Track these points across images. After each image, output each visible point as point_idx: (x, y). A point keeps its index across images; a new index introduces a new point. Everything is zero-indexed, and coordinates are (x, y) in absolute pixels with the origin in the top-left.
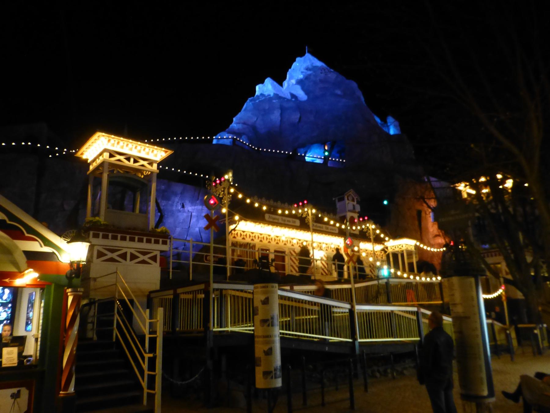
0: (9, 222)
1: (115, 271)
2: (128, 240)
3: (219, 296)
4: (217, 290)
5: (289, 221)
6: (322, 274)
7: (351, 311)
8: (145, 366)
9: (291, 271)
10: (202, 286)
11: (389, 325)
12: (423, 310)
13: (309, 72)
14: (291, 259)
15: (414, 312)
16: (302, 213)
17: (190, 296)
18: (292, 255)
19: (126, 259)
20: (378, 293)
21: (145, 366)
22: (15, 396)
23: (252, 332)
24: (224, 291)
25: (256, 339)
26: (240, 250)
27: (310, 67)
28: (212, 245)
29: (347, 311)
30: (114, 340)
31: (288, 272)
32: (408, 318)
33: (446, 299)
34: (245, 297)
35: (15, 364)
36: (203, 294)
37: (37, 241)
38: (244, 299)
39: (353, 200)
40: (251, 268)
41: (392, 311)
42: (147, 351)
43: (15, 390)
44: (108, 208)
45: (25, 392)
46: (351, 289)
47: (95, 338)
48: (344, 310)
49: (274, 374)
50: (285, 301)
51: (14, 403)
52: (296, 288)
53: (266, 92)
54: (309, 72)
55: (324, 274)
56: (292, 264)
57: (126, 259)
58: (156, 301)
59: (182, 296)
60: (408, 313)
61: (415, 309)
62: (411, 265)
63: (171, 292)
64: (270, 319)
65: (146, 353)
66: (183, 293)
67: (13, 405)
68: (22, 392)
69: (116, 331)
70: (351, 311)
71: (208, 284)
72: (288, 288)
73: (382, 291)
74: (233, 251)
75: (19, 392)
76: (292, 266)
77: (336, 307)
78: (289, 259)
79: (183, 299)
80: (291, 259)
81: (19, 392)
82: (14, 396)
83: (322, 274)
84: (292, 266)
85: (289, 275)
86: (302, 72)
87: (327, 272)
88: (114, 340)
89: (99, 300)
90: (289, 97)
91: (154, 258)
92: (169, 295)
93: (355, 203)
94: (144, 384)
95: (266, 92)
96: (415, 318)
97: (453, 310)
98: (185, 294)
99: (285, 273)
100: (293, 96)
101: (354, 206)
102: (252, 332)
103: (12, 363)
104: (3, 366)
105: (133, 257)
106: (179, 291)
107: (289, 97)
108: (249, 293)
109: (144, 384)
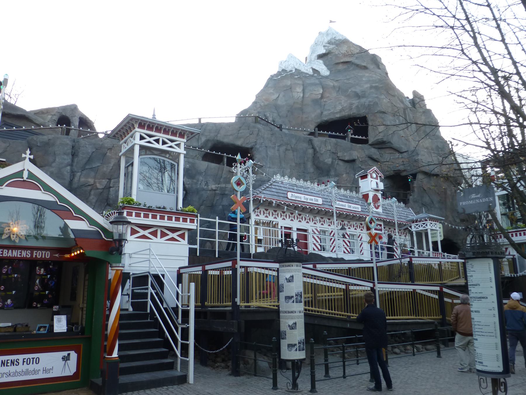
0: (59, 203)
1: (149, 248)
2: (190, 247)
3: (342, 297)
4: (243, 267)
5: (312, 200)
6: (344, 252)
7: (373, 289)
8: (179, 337)
9: (314, 250)
10: (229, 264)
11: (410, 302)
12: (445, 290)
13: (331, 47)
14: (313, 237)
15: (436, 291)
17: (217, 273)
18: (315, 233)
19: (156, 237)
20: (400, 271)
21: (179, 337)
22: (66, 359)
23: (277, 308)
24: (248, 268)
25: (281, 314)
26: (263, 229)
27: (333, 41)
28: (238, 224)
29: (369, 289)
30: (149, 311)
31: (310, 250)
32: (427, 296)
35: (65, 330)
36: (441, 315)
37: (84, 220)
39: (377, 178)
40: (274, 246)
42: (180, 322)
43: (65, 353)
45: (74, 355)
47: (131, 309)
48: (366, 288)
49: (298, 346)
50: (434, 295)
51: (65, 364)
53: (287, 68)
54: (331, 47)
56: (315, 242)
57: (156, 237)
58: (185, 277)
59: (210, 273)
60: (433, 293)
61: (438, 288)
62: (435, 243)
63: (200, 268)
64: (295, 296)
65: (179, 324)
66: (211, 270)
67: (479, 81)
68: (71, 355)
69: (150, 302)
71: (235, 262)
72: (311, 266)
73: (405, 270)
74: (256, 229)
75: (69, 354)
76: (315, 244)
78: (312, 236)
80: (313, 237)
81: (69, 354)
82: (64, 358)
83: (344, 252)
84: (315, 244)
85: (311, 254)
86: (324, 46)
87: (349, 250)
88: (149, 311)
89: (133, 274)
90: (311, 72)
91: (182, 236)
92: (198, 270)
93: (378, 181)
94: (178, 353)
95: (287, 68)
96: (437, 297)
97: (471, 290)
98: (213, 270)
99: (307, 252)
100: (314, 70)
101: (377, 183)
102: (277, 308)
103: (62, 329)
104: (55, 331)
105: (163, 235)
106: (207, 267)
107: (311, 72)
108: (274, 270)
109: (178, 353)
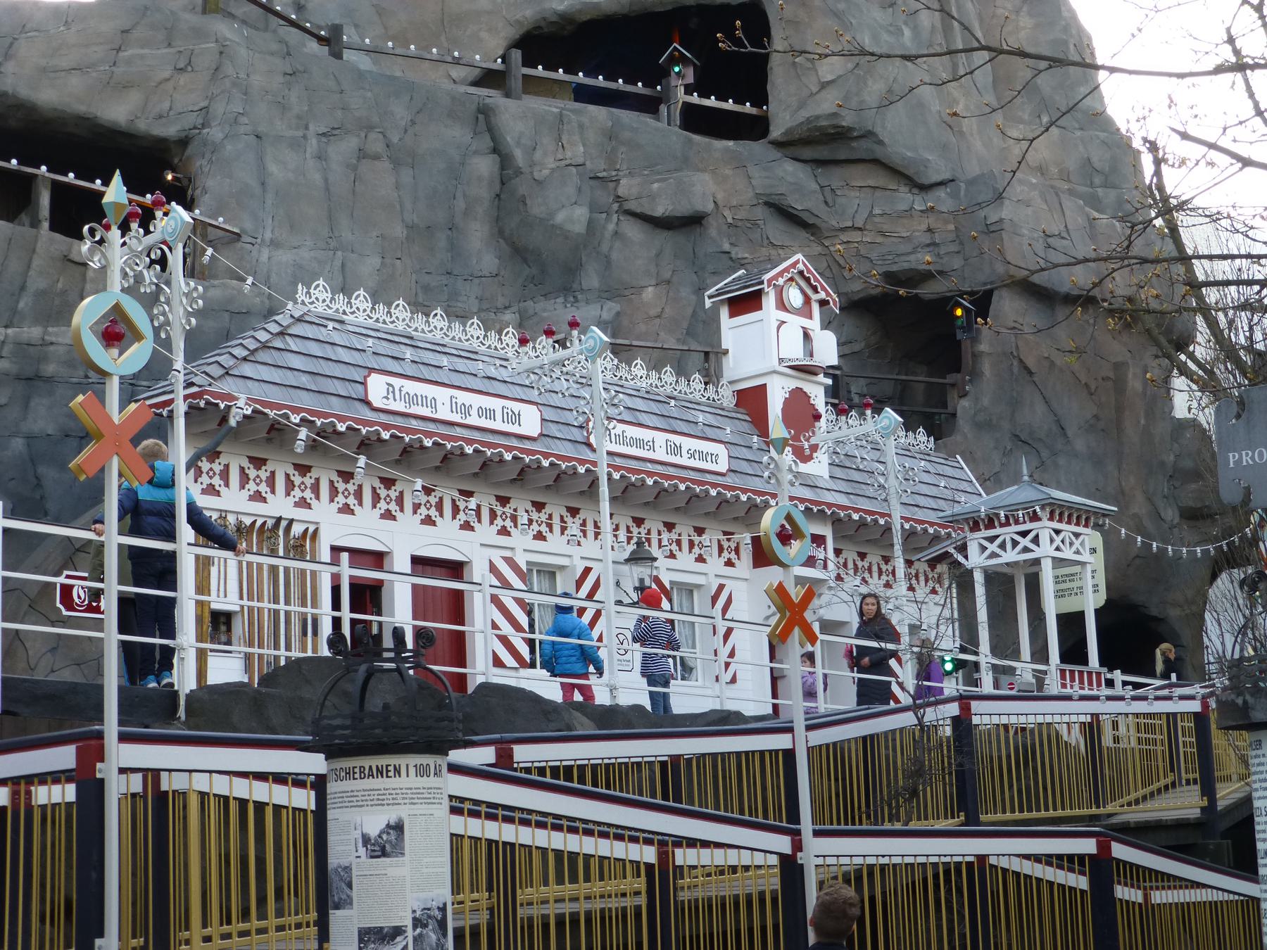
5: (490, 414)
7: (790, 868)
12: (1119, 851)
15: (1081, 858)
16: (1229, 494)
24: (164, 775)
32: (1062, 887)
33: (1226, 794)
34: (486, 840)
38: (551, 856)
40: (296, 654)
41: (982, 858)
44: (1082, 588)
46: (790, 755)
52: (524, 754)
55: (508, 660)
56: (507, 629)
61: (1088, 846)
70: (790, 868)
71: (92, 750)
72: (483, 756)
77: (692, 843)
79: (689, 901)
84: (504, 640)
85: (486, 688)
93: (814, 324)
101: (807, 336)
